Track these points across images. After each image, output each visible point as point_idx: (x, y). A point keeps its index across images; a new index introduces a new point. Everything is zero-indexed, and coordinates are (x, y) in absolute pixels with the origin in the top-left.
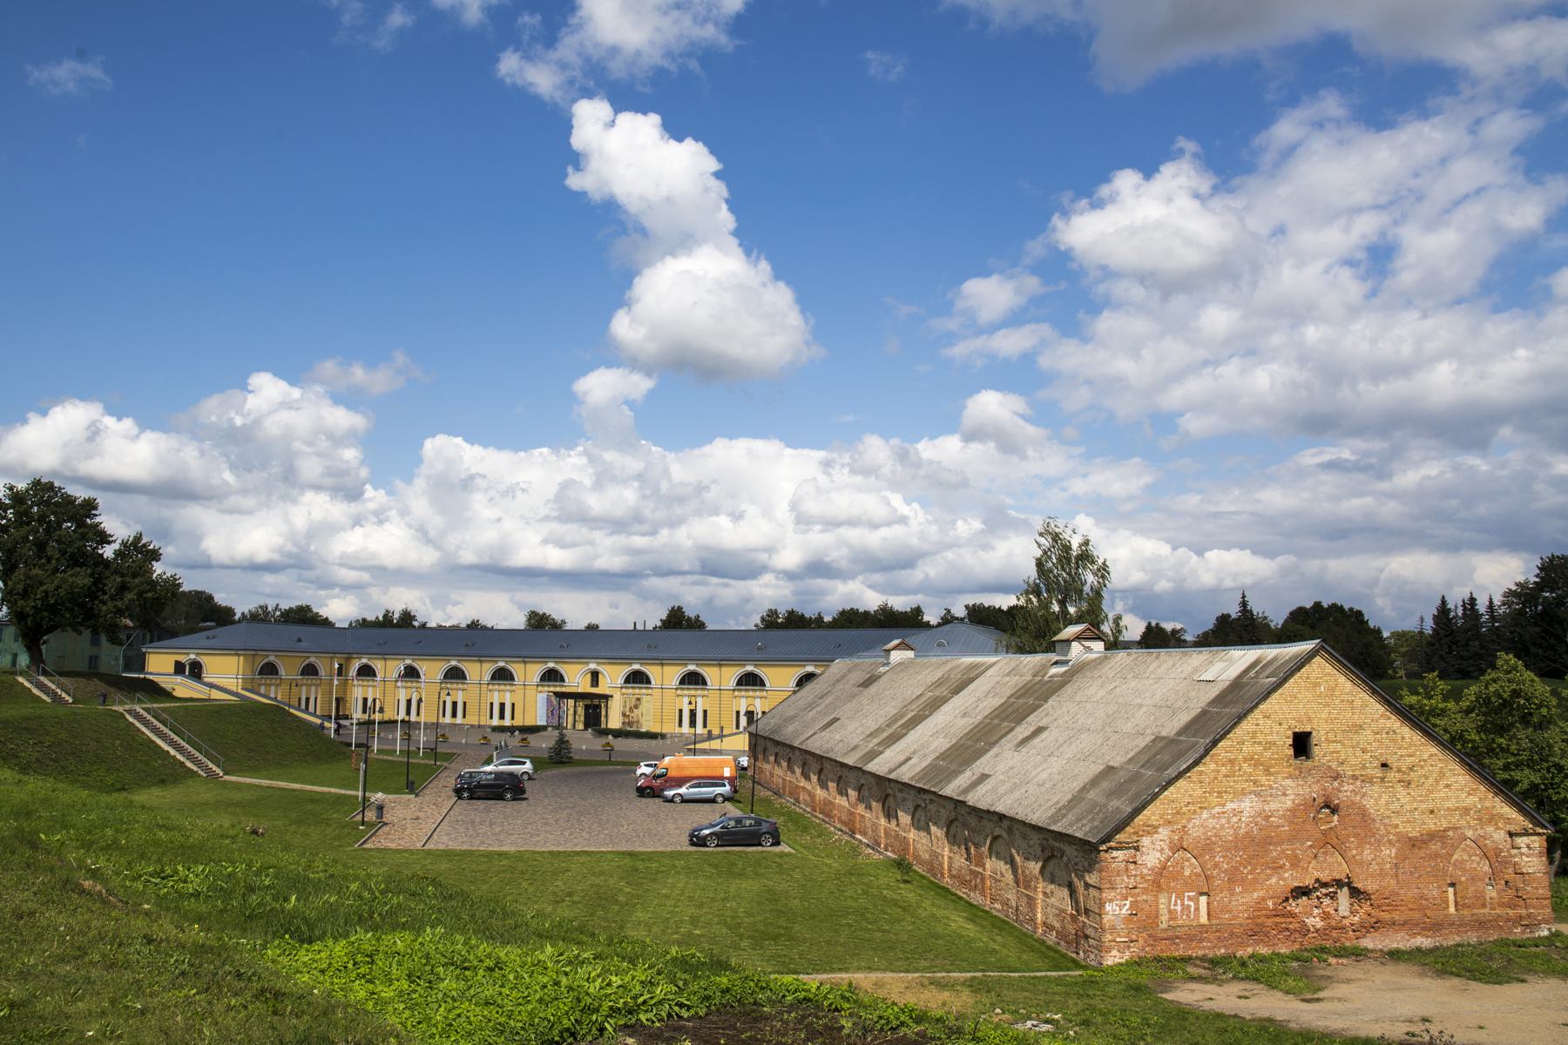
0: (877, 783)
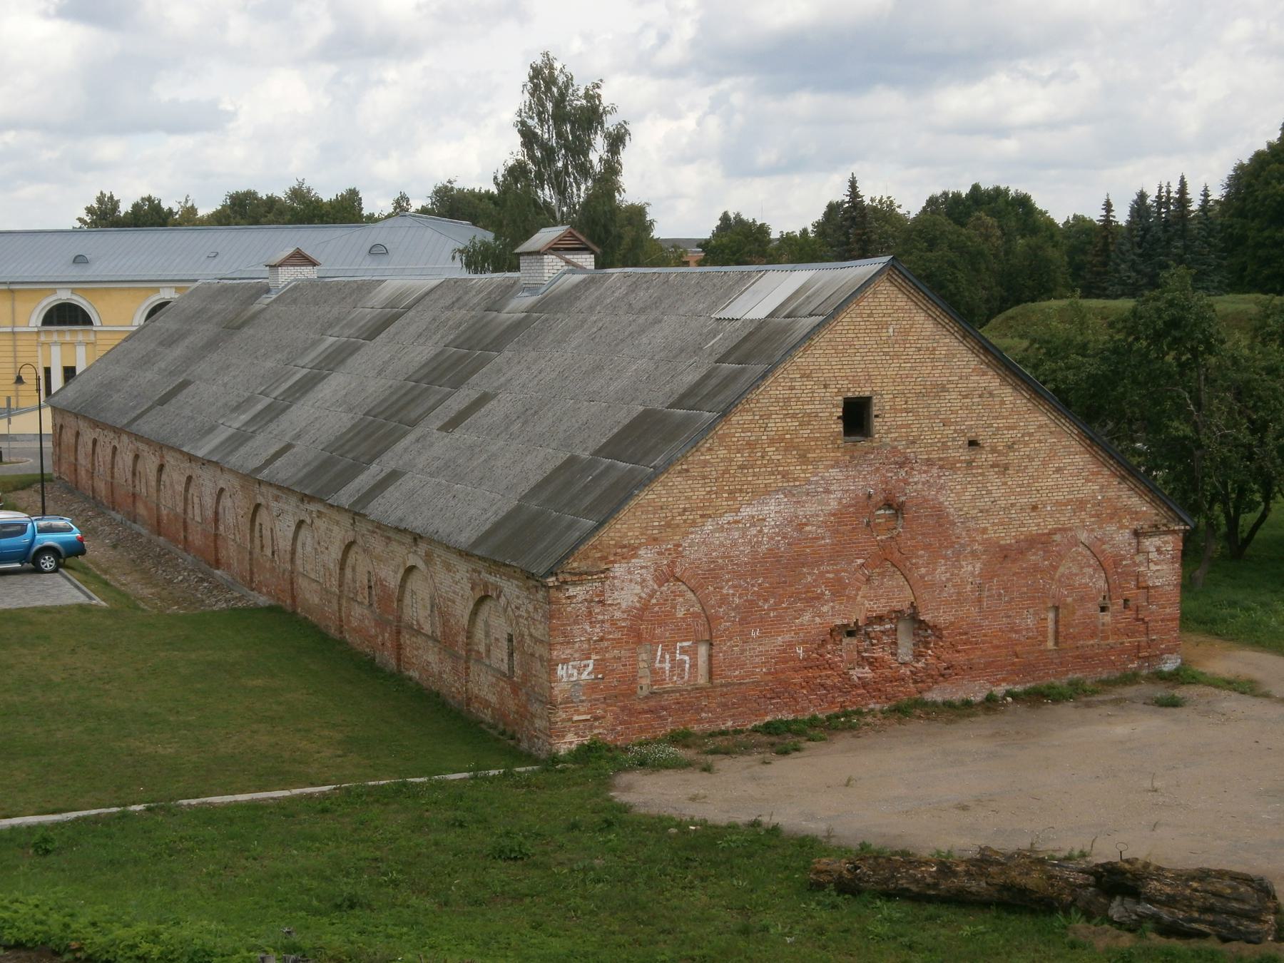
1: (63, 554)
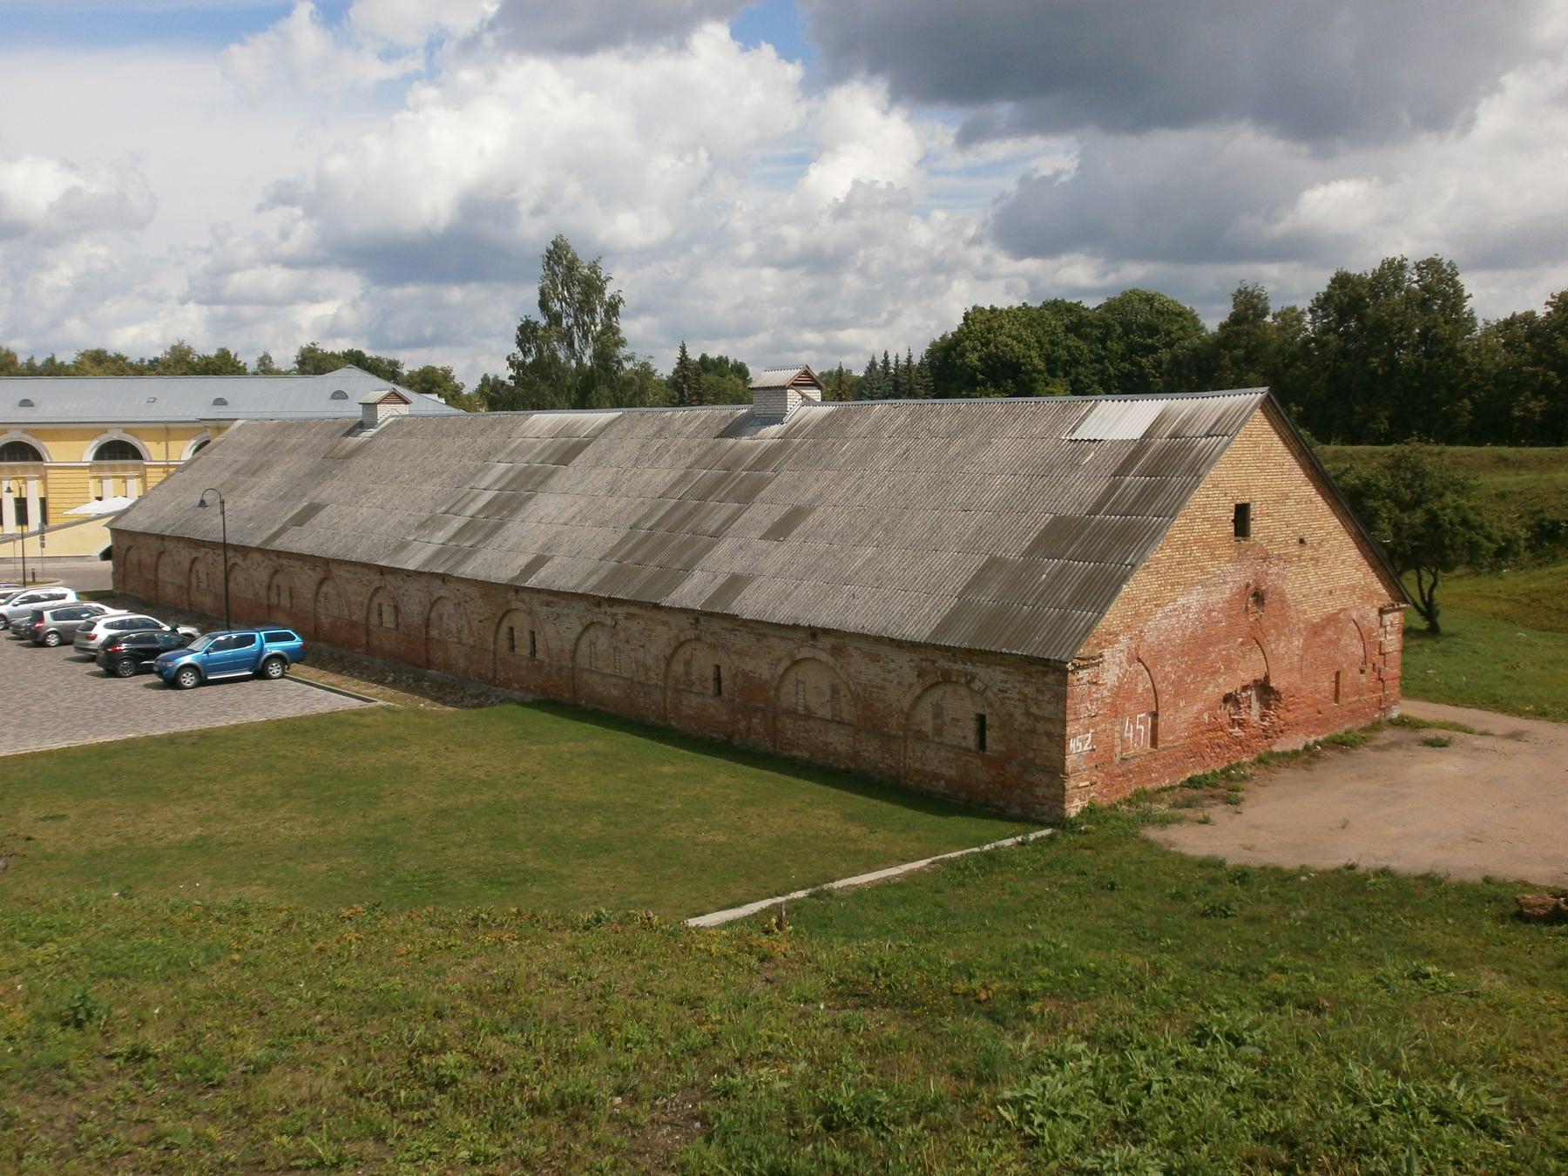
0: (484, 596)
1: (288, 659)
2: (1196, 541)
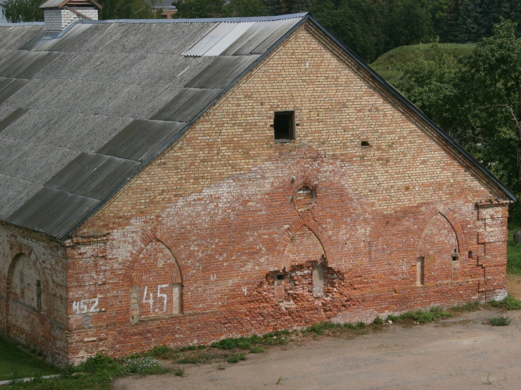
2: (224, 143)
